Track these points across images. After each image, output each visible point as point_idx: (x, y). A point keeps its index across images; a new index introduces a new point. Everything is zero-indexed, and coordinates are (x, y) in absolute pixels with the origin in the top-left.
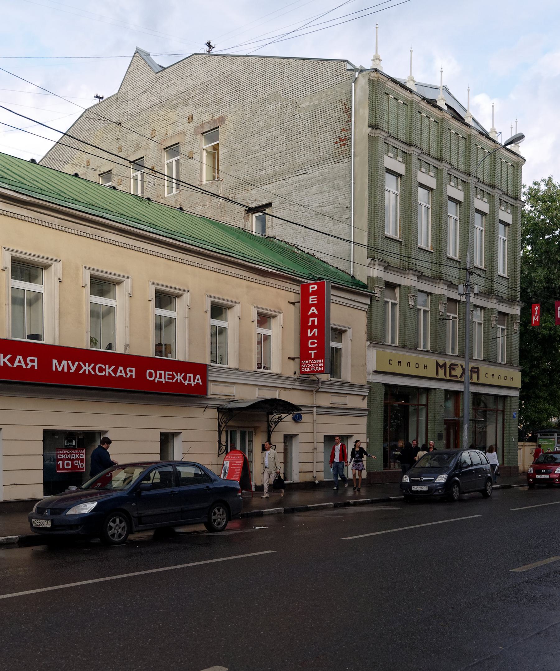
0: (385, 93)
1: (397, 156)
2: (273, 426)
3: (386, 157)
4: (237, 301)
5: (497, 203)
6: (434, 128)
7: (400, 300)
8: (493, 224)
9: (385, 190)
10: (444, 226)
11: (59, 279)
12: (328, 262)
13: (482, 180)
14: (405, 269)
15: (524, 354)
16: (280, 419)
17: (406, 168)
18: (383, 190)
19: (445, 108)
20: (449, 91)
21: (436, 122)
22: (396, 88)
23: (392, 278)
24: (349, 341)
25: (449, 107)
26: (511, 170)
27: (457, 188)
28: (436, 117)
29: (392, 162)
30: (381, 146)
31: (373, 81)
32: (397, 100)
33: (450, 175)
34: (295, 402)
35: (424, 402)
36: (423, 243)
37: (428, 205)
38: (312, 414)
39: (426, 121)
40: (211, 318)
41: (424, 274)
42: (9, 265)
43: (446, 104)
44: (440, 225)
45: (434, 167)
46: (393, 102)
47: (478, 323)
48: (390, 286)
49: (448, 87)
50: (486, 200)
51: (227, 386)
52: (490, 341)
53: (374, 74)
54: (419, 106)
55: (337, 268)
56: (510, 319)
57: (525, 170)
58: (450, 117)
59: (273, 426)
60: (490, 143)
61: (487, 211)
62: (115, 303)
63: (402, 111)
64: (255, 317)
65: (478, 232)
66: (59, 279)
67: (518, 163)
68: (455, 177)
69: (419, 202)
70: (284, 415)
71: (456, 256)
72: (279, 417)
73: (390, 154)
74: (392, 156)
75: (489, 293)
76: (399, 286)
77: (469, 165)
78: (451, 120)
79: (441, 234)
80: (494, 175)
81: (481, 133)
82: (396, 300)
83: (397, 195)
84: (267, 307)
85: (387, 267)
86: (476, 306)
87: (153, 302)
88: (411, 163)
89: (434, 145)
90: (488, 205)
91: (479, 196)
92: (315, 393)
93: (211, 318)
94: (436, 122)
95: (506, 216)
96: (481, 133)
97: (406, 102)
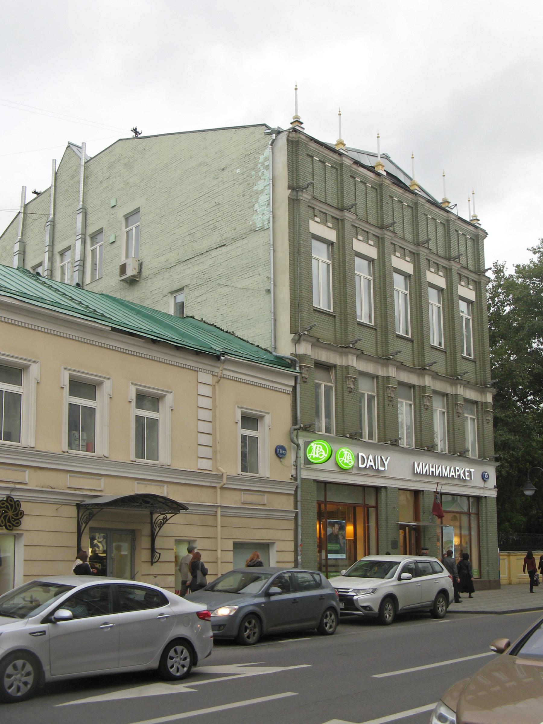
0: (308, 155)
1: (326, 221)
2: (158, 529)
3: (393, 257)
4: (36, 360)
5: (455, 277)
6: (372, 195)
7: (336, 383)
8: (452, 300)
9: (394, 289)
10: (389, 300)
11: (36, 379)
12: (248, 340)
13: (434, 250)
14: (345, 348)
15: (500, 446)
16: (165, 520)
17: (338, 235)
18: (309, 258)
19: (385, 174)
20: (391, 159)
21: (335, 168)
22: (321, 150)
23: (325, 356)
24: (267, 429)
25: (388, 173)
26: (470, 243)
27: (438, 274)
28: (470, 233)
29: (402, 263)
30: (303, 209)
31: (292, 141)
32: (427, 215)
33: (395, 245)
34: (179, 500)
35: (373, 503)
36: (363, 317)
37: (438, 305)
38: (215, 515)
39: (362, 187)
40: (70, 395)
41: (365, 353)
42: (67, 383)
43: (385, 171)
44: (385, 298)
45: (373, 235)
46: (318, 166)
47: (471, 418)
48: (324, 367)
49: (390, 155)
50: (471, 287)
51: (18, 470)
52: (455, 433)
53: (294, 134)
54: (351, 170)
55: (258, 346)
56: (480, 407)
57: (488, 244)
58: (390, 183)
59: (158, 529)
60: (442, 212)
61: (473, 298)
62: (95, 405)
63: (331, 175)
64: (133, 396)
65: (401, 297)
66: (36, 379)
67: (477, 236)
68: (400, 247)
69: (356, 272)
70: (169, 516)
71: (407, 334)
72: (164, 518)
73: (398, 254)
74: (399, 256)
75: (454, 378)
76: (335, 366)
77: (418, 235)
78: (392, 186)
79: (386, 308)
80: (450, 248)
81: (428, 201)
82: (331, 382)
83: (406, 295)
84: (253, 408)
85: (317, 343)
86: (435, 392)
87: (67, 389)
88: (343, 228)
89: (372, 211)
90: (474, 293)
91: (463, 283)
92: (219, 490)
93: (70, 395)
94: (335, 168)
95: (467, 292)
96: (428, 201)
97: (334, 166)
